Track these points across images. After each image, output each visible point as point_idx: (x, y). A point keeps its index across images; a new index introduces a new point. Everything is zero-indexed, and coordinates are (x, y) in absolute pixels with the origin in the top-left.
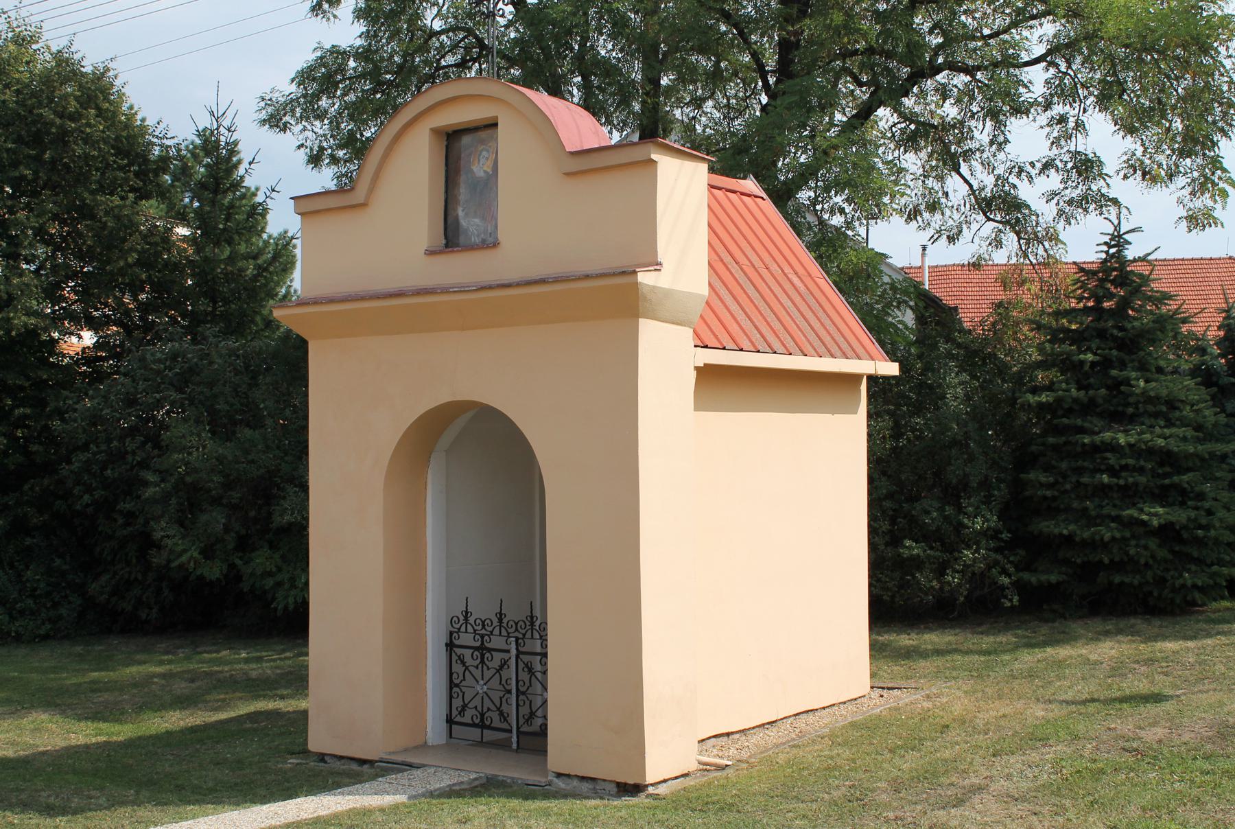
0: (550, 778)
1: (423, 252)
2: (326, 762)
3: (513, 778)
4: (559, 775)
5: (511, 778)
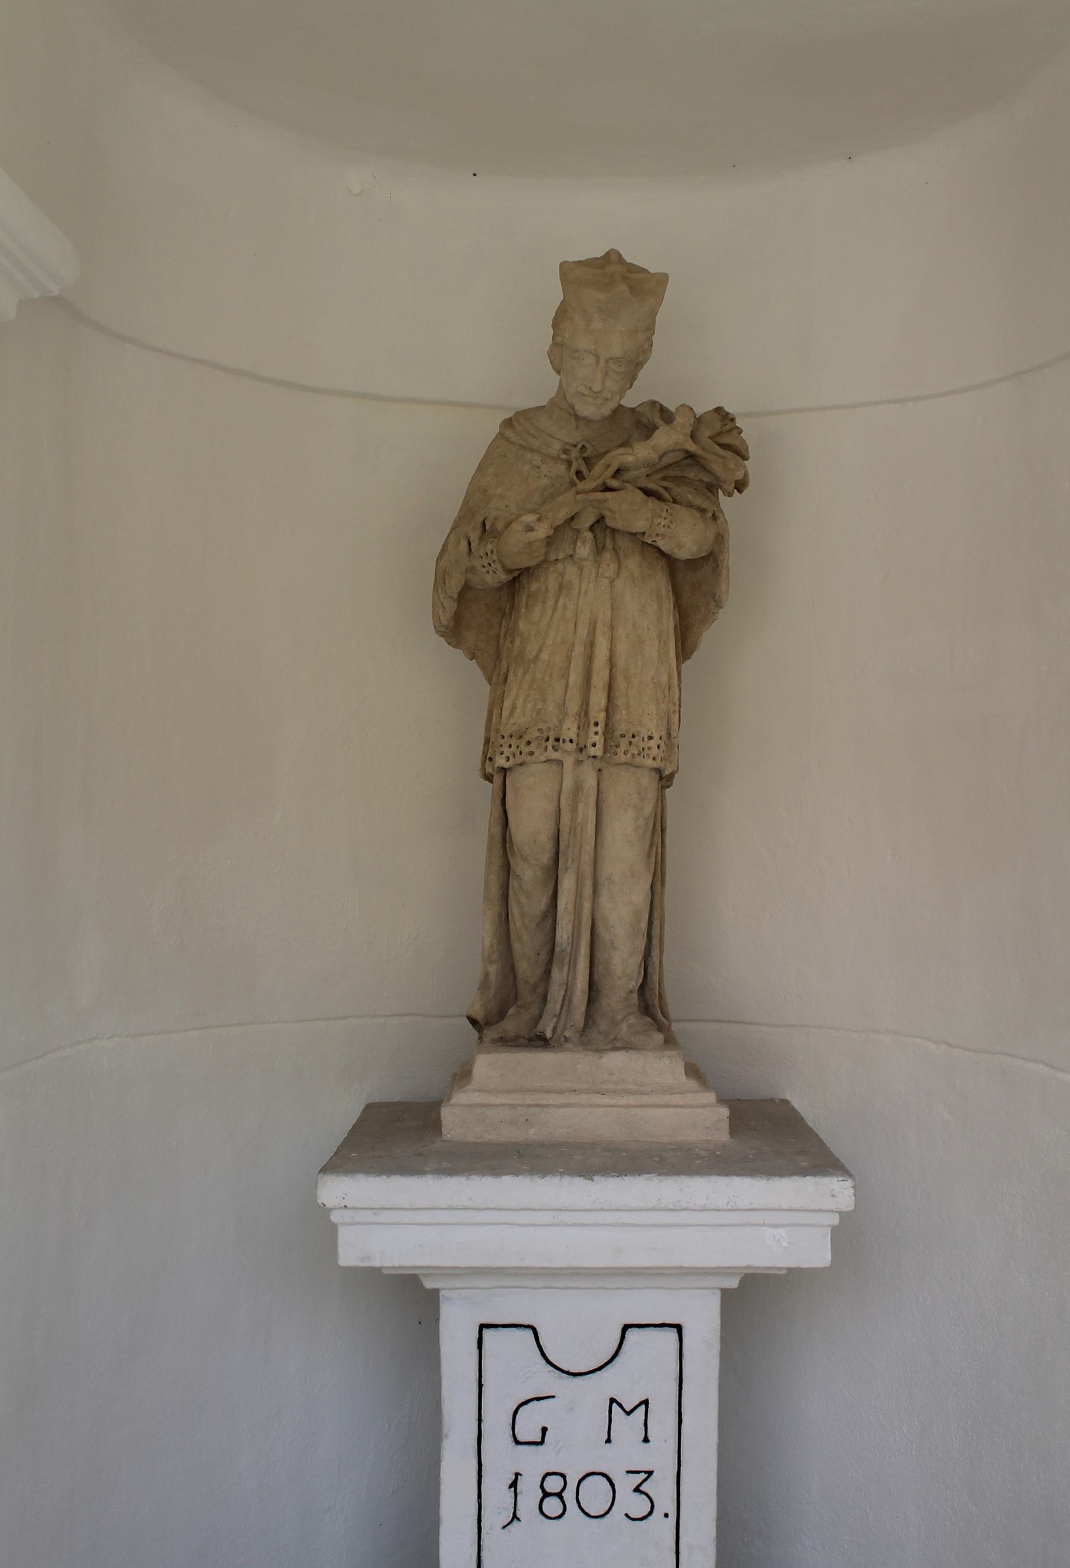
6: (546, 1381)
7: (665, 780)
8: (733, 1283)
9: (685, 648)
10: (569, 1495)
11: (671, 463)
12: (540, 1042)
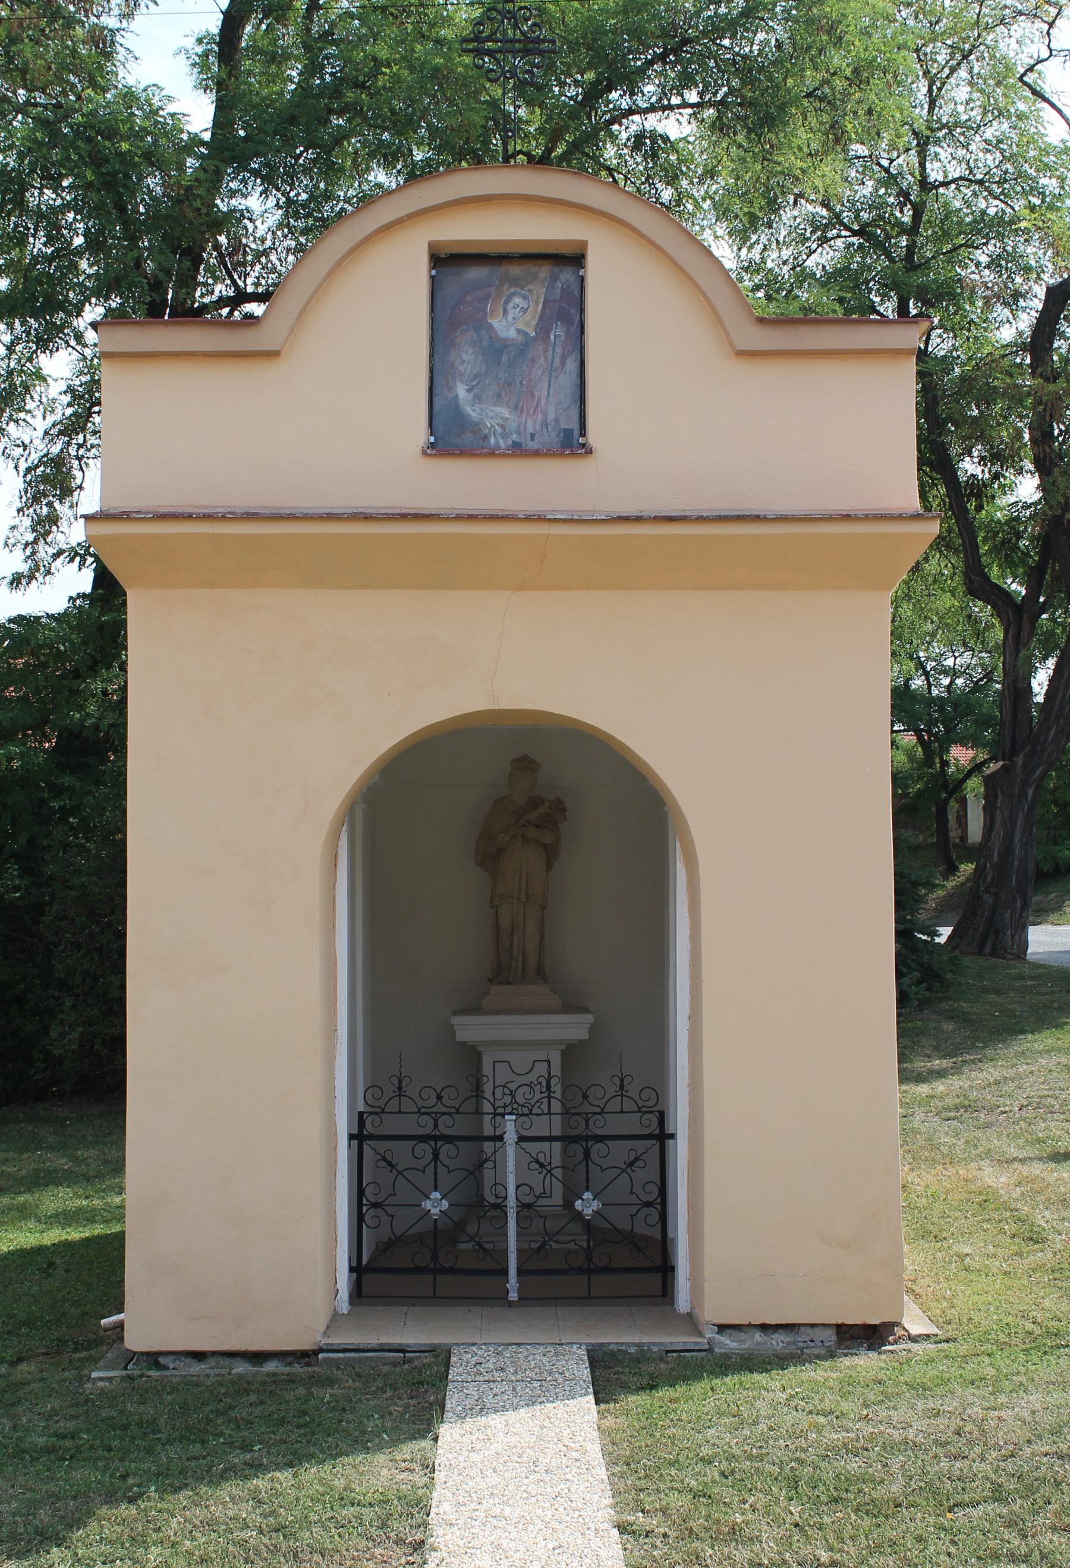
0: (708, 1336)
1: (419, 450)
2: (165, 1368)
3: (638, 1345)
4: (722, 1328)
5: (635, 1344)
6: (513, 1077)
7: (543, 908)
8: (564, 1048)
9: (549, 867)
10: (526, 1080)
11: (214, 24)
12: (509, 983)
